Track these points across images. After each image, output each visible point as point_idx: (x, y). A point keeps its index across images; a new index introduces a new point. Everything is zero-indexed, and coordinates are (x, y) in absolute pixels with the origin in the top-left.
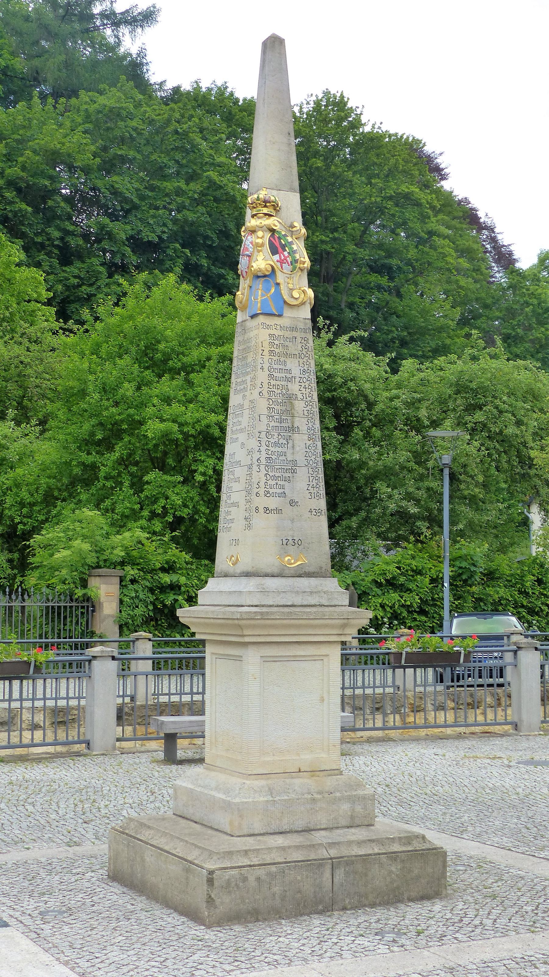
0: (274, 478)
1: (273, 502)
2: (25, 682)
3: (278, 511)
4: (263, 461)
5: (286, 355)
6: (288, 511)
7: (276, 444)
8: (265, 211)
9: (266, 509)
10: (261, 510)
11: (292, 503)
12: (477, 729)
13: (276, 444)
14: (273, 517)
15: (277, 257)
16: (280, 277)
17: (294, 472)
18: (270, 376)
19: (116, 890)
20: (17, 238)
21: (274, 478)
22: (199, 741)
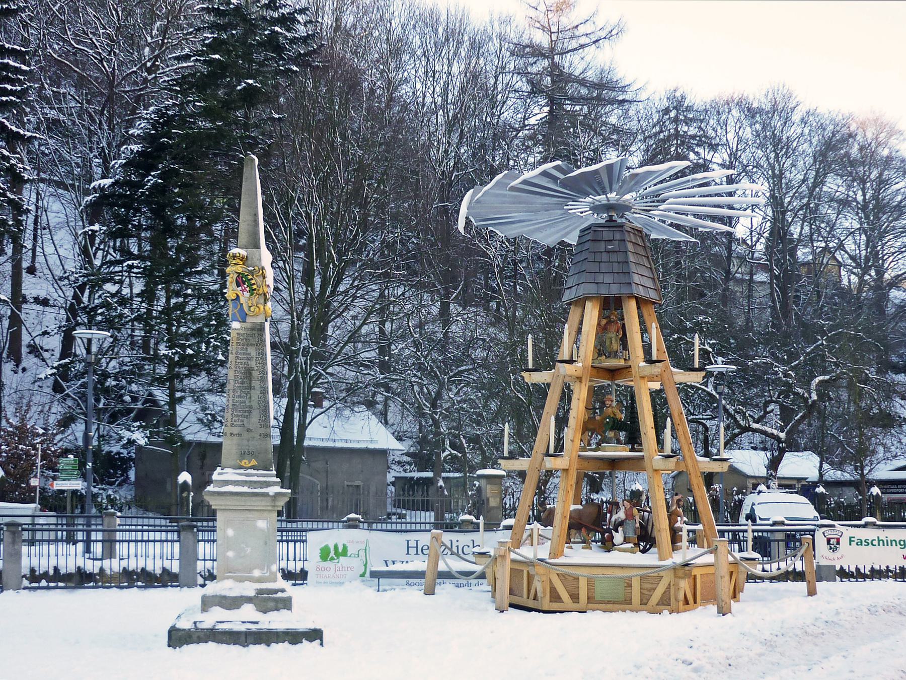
0: (238, 416)
1: (236, 430)
2: (298, 544)
3: (239, 435)
4: (230, 406)
5: (248, 345)
6: (246, 435)
7: (239, 396)
8: (234, 262)
9: (231, 434)
10: (228, 434)
11: (249, 430)
12: (327, 580)
13: (239, 396)
14: (235, 438)
15: (240, 288)
16: (242, 300)
17: (250, 412)
18: (237, 357)
19: (361, 410)
20: (200, 444)
21: (238, 416)
22: (596, 364)
